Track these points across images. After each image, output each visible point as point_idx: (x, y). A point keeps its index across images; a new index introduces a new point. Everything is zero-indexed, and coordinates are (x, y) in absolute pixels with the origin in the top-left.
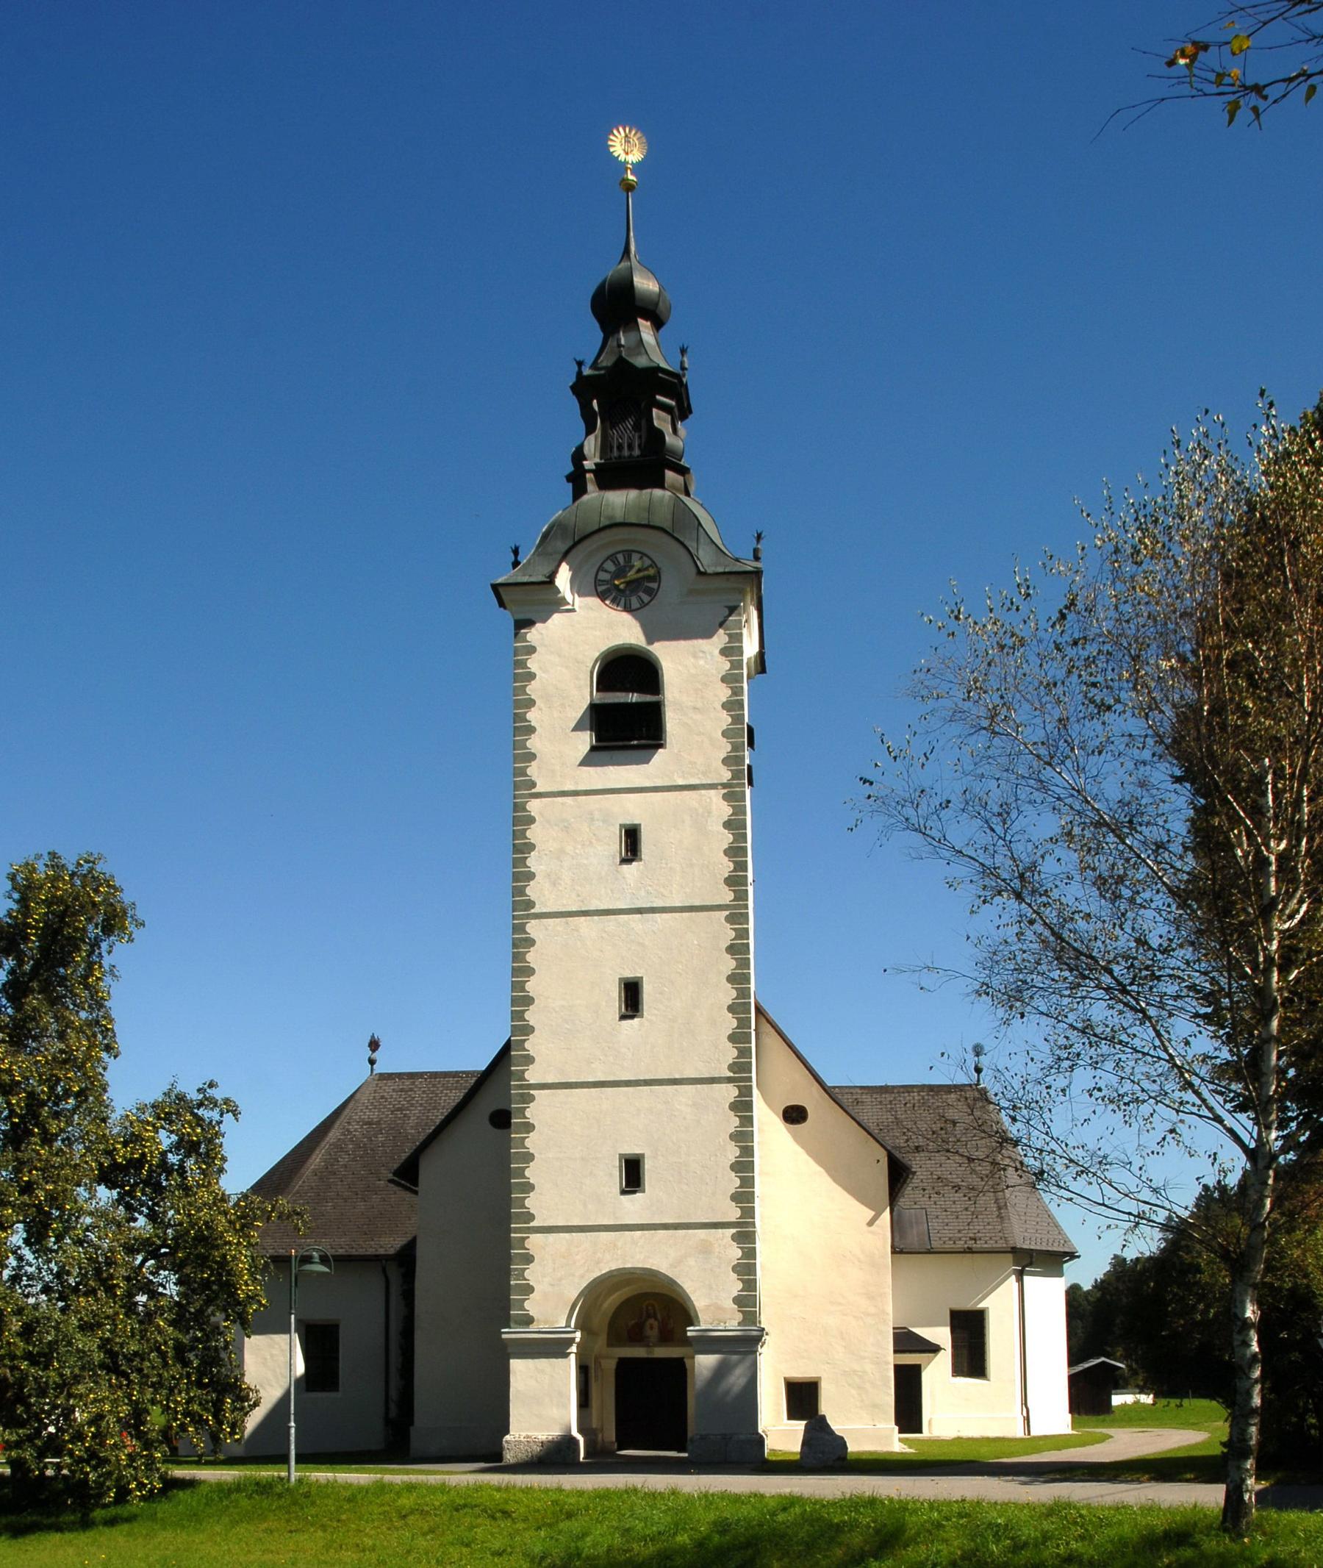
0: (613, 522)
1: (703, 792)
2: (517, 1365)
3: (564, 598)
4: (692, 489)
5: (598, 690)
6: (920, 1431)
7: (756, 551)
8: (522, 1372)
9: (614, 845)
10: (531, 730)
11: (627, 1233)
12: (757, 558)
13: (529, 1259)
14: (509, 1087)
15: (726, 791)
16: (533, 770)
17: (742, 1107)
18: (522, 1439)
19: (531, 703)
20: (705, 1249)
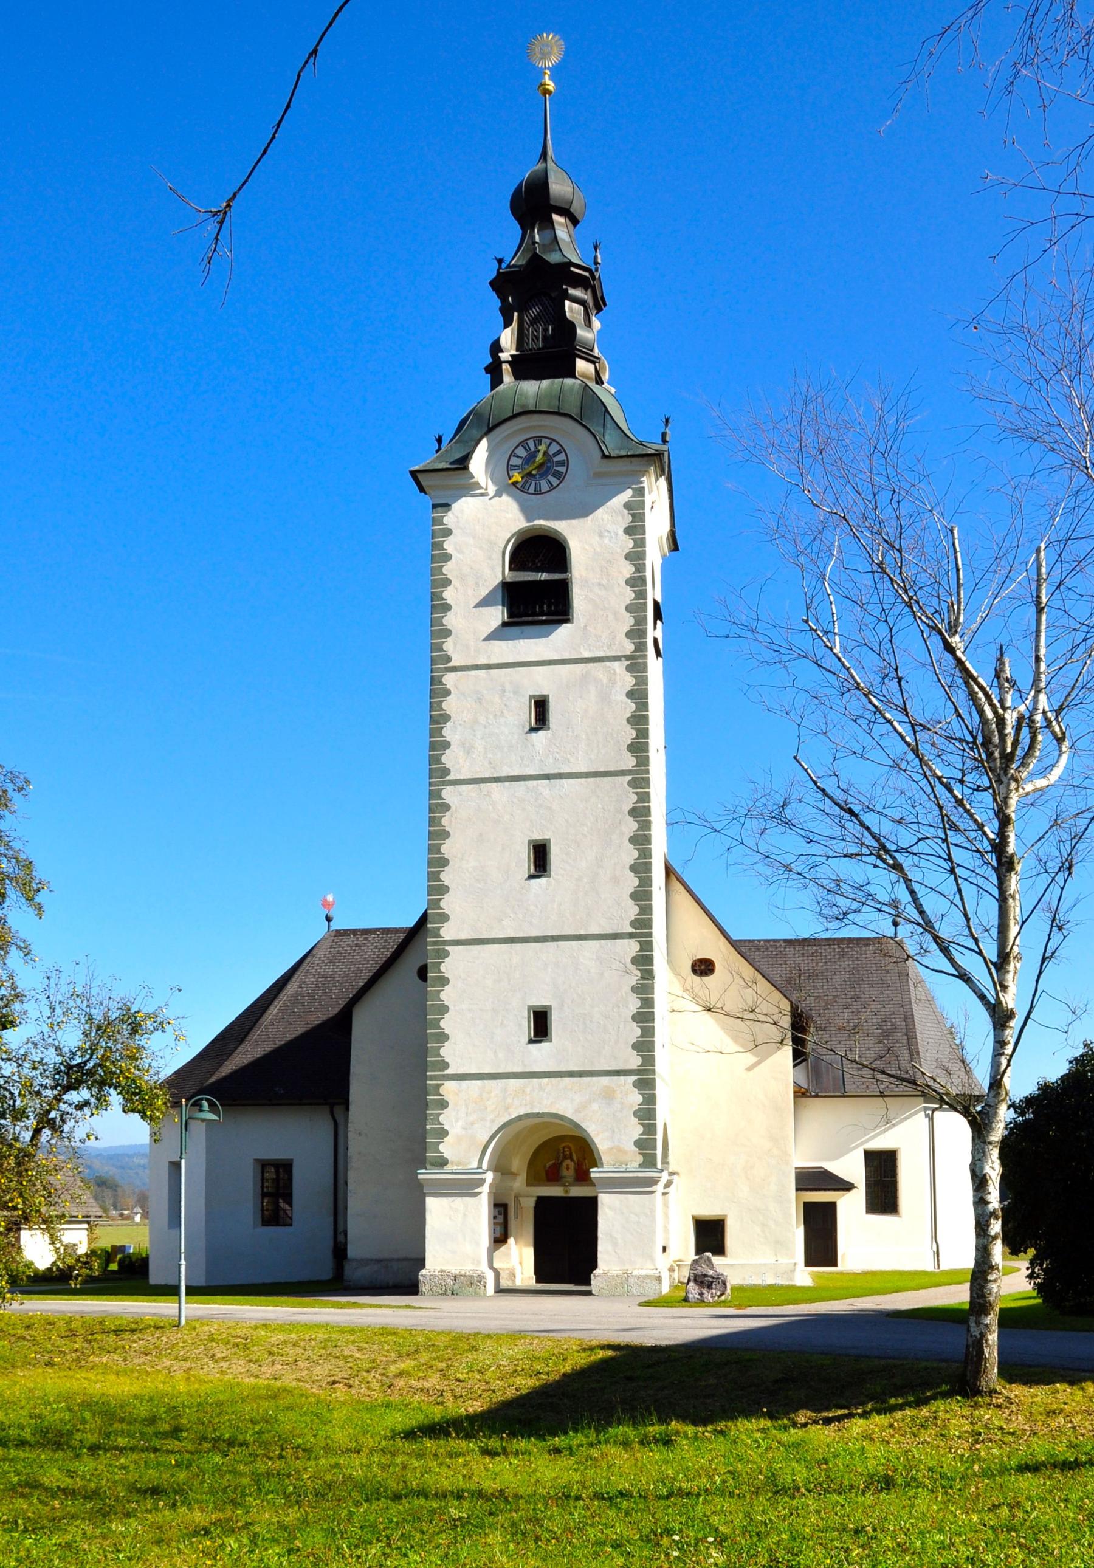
0: (526, 409)
1: (608, 664)
2: (431, 1203)
3: (477, 483)
4: (606, 377)
5: (510, 569)
6: (835, 1264)
7: (664, 435)
8: (436, 1209)
9: (526, 714)
10: (447, 608)
11: (535, 1080)
12: (664, 441)
13: (443, 1105)
14: (426, 944)
15: (629, 662)
16: (449, 646)
17: (644, 961)
18: (437, 1273)
19: (447, 582)
20: (608, 1095)
